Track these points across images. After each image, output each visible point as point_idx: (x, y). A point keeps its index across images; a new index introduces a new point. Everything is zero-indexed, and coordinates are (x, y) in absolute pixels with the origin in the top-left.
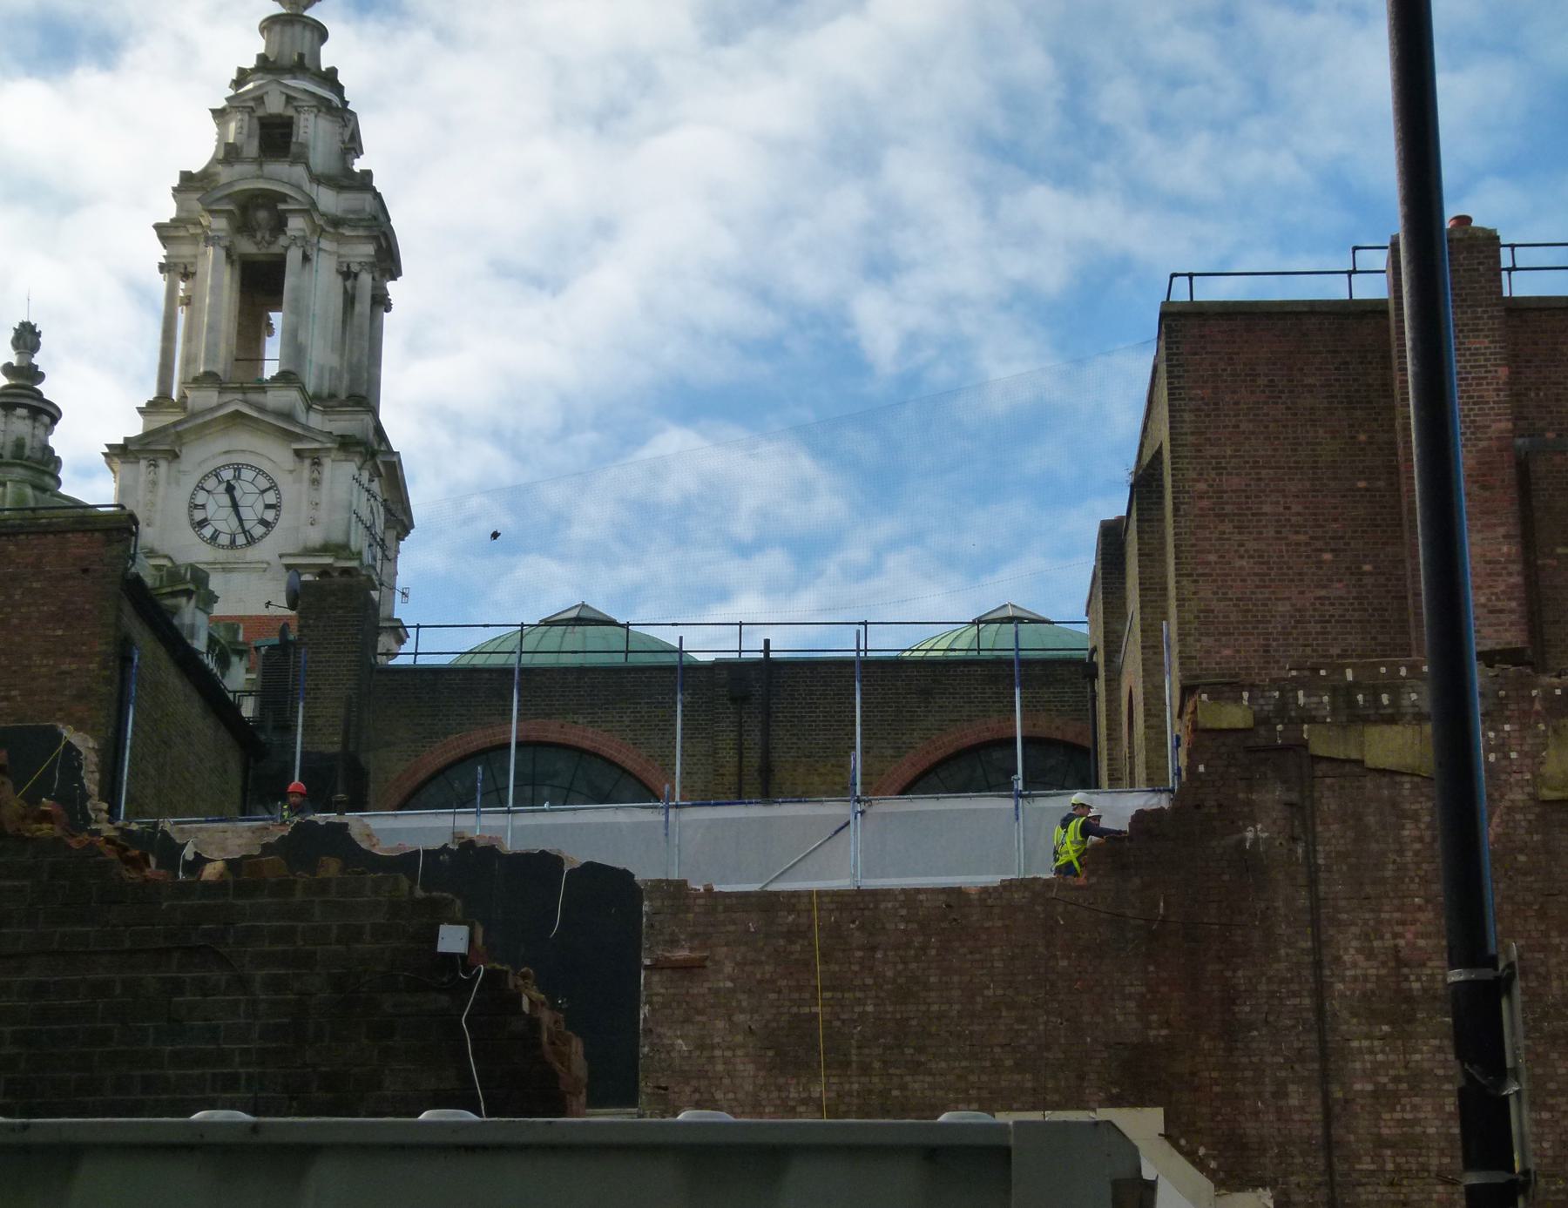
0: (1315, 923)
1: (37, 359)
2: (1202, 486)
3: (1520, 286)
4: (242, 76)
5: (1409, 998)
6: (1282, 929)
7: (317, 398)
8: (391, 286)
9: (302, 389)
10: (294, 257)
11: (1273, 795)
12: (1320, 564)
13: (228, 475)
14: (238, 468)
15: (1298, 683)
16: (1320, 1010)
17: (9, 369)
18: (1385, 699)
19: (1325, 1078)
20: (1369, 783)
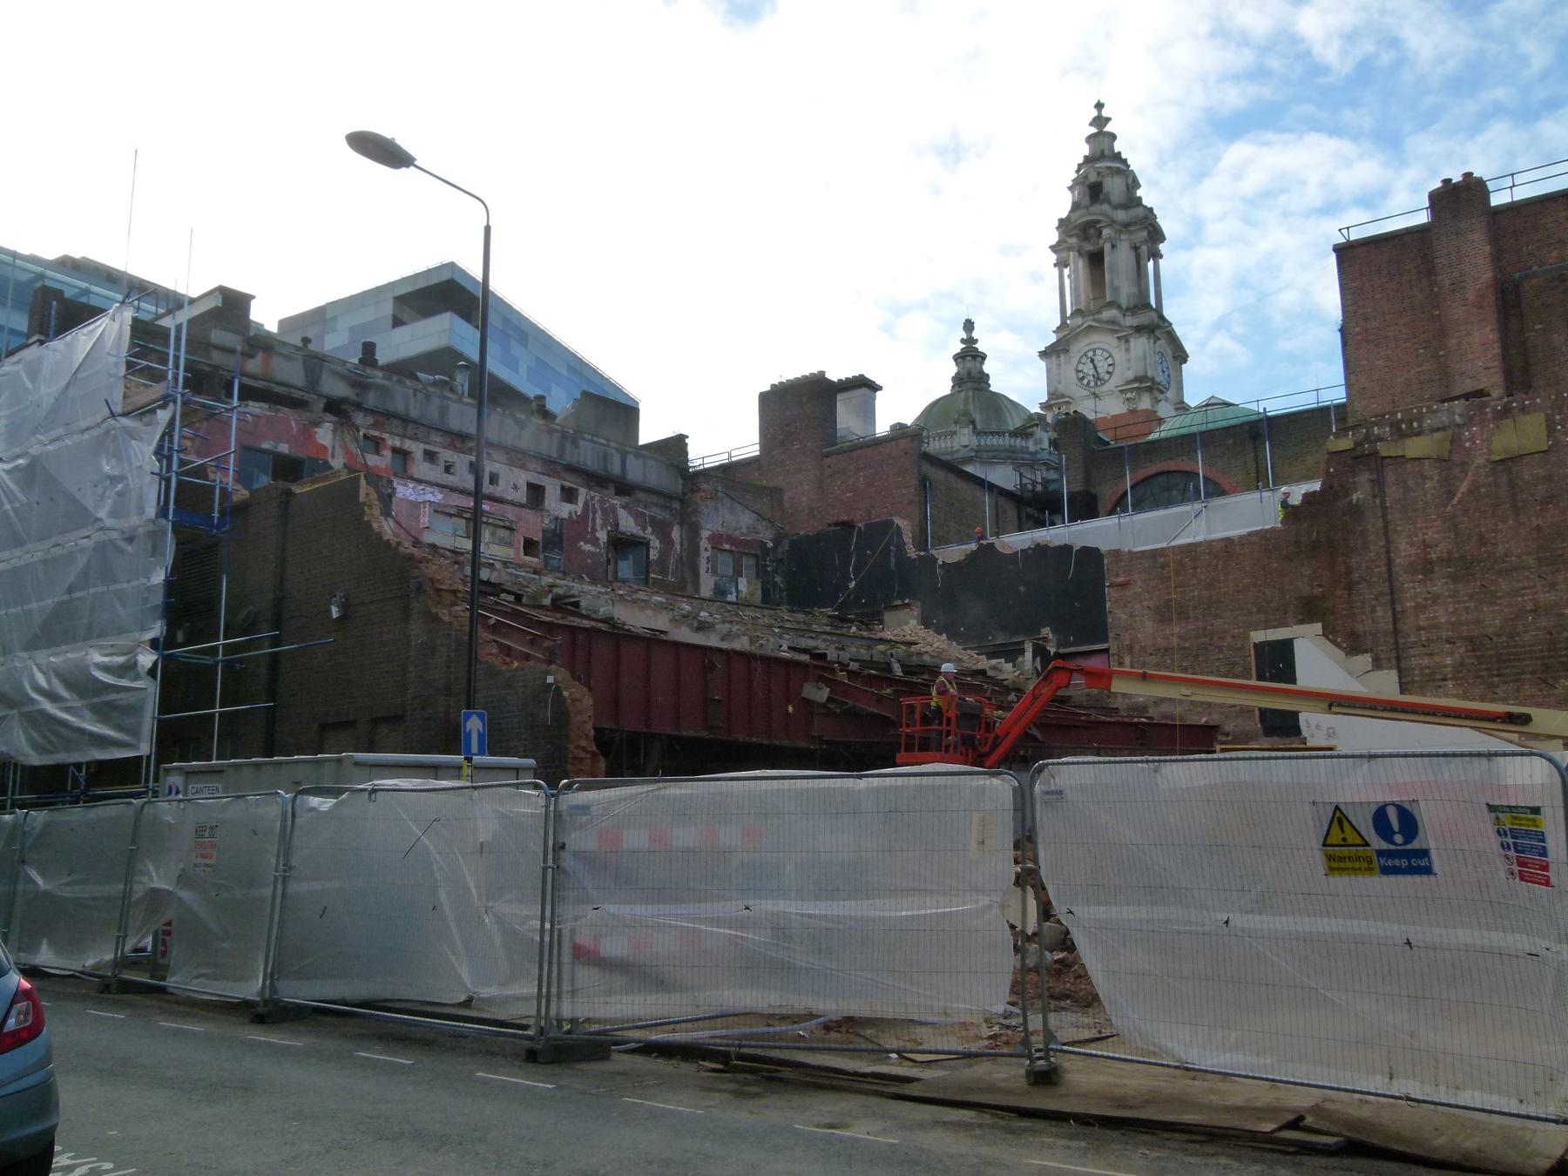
0: (1386, 533)
1: (975, 335)
3: (1496, 200)
4: (1080, 166)
5: (1431, 562)
6: (1372, 538)
7: (1128, 309)
8: (1161, 246)
9: (1119, 307)
10: (1107, 247)
11: (1364, 478)
12: (1417, 356)
13: (1090, 354)
15: (1375, 423)
16: (1390, 571)
17: (963, 341)
19: (1393, 602)
20: (1409, 466)
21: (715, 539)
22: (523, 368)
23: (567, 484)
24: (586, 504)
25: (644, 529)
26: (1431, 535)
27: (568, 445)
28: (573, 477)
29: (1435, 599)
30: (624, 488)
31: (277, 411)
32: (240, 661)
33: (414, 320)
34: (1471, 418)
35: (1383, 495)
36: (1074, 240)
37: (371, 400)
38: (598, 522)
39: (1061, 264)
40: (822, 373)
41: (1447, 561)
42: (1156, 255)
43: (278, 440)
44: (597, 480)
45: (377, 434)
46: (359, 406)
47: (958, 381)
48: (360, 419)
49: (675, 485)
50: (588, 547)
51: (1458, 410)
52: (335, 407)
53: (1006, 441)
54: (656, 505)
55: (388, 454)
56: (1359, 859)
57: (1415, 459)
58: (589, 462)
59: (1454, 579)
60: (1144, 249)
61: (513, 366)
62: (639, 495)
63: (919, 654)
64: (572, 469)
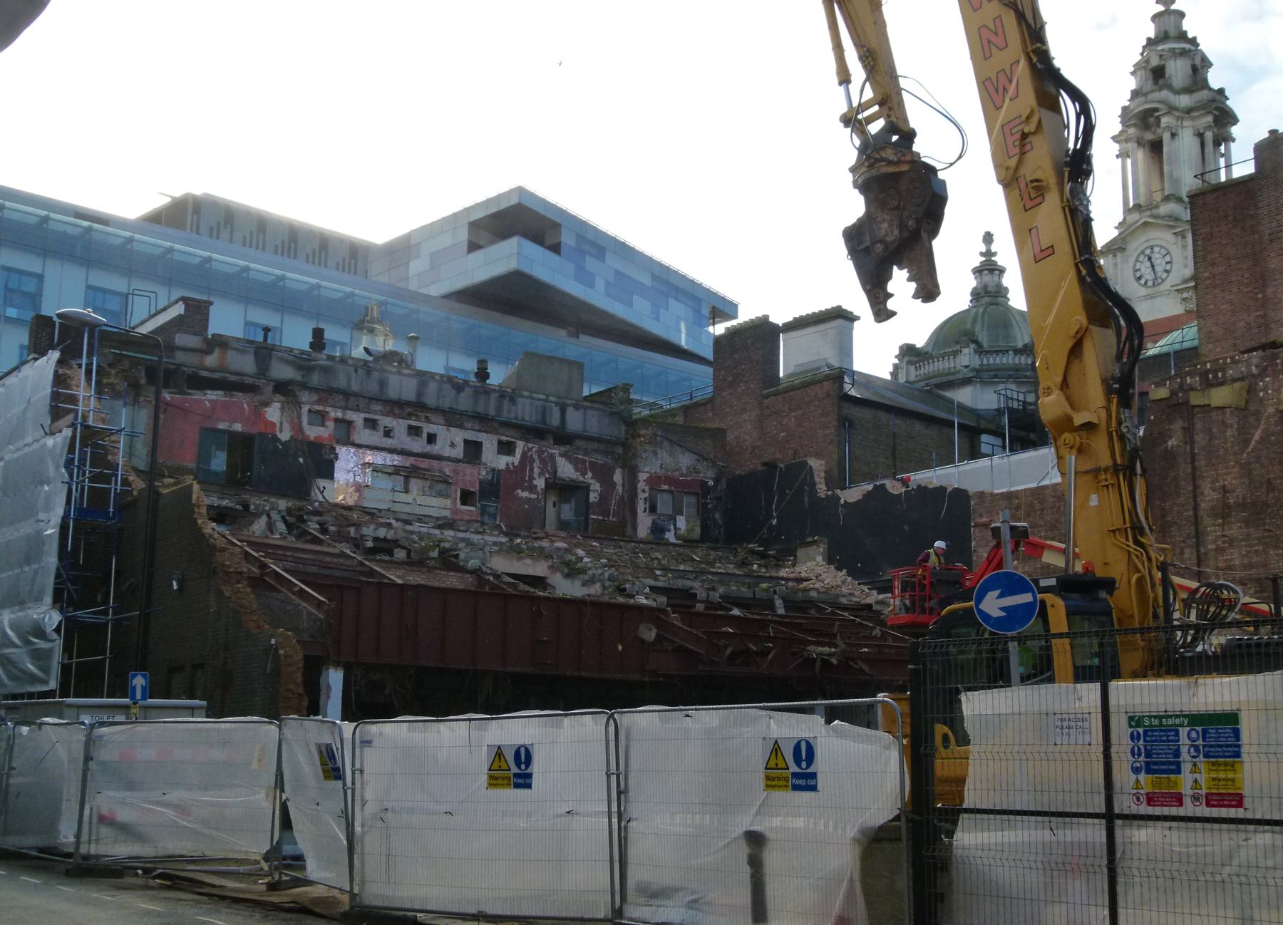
2: (1206, 274)
4: (1144, 47)
6: (1182, 483)
10: (1166, 137)
11: (1178, 425)
12: (1257, 299)
13: (1148, 252)
14: (1152, 248)
16: (1196, 516)
17: (982, 254)
18: (1220, 375)
19: (1198, 545)
20: (1214, 414)
21: (654, 481)
22: (600, 284)
23: (504, 438)
24: (524, 455)
25: (584, 474)
26: (1230, 481)
27: (506, 403)
28: (511, 432)
29: (1231, 542)
30: (563, 438)
31: (232, 396)
32: (125, 619)
33: (492, 243)
34: (1265, 369)
35: (1192, 443)
36: (1132, 131)
37: (315, 379)
38: (536, 470)
39: (1122, 155)
40: (766, 317)
41: (1242, 506)
42: (1228, 139)
43: (233, 421)
44: (535, 433)
45: (321, 408)
46: (304, 386)
47: (976, 295)
48: (304, 396)
49: (620, 431)
50: (525, 494)
51: (1255, 361)
52: (283, 388)
53: (1009, 359)
54: (596, 451)
55: (331, 424)
56: (779, 778)
57: (1218, 408)
58: (527, 418)
59: (1247, 523)
60: (1209, 136)
61: (586, 278)
62: (578, 443)
63: (805, 590)
64: (507, 425)
